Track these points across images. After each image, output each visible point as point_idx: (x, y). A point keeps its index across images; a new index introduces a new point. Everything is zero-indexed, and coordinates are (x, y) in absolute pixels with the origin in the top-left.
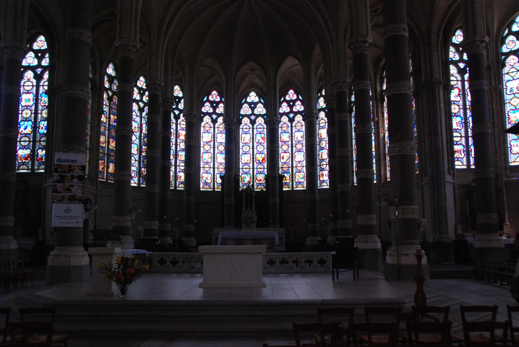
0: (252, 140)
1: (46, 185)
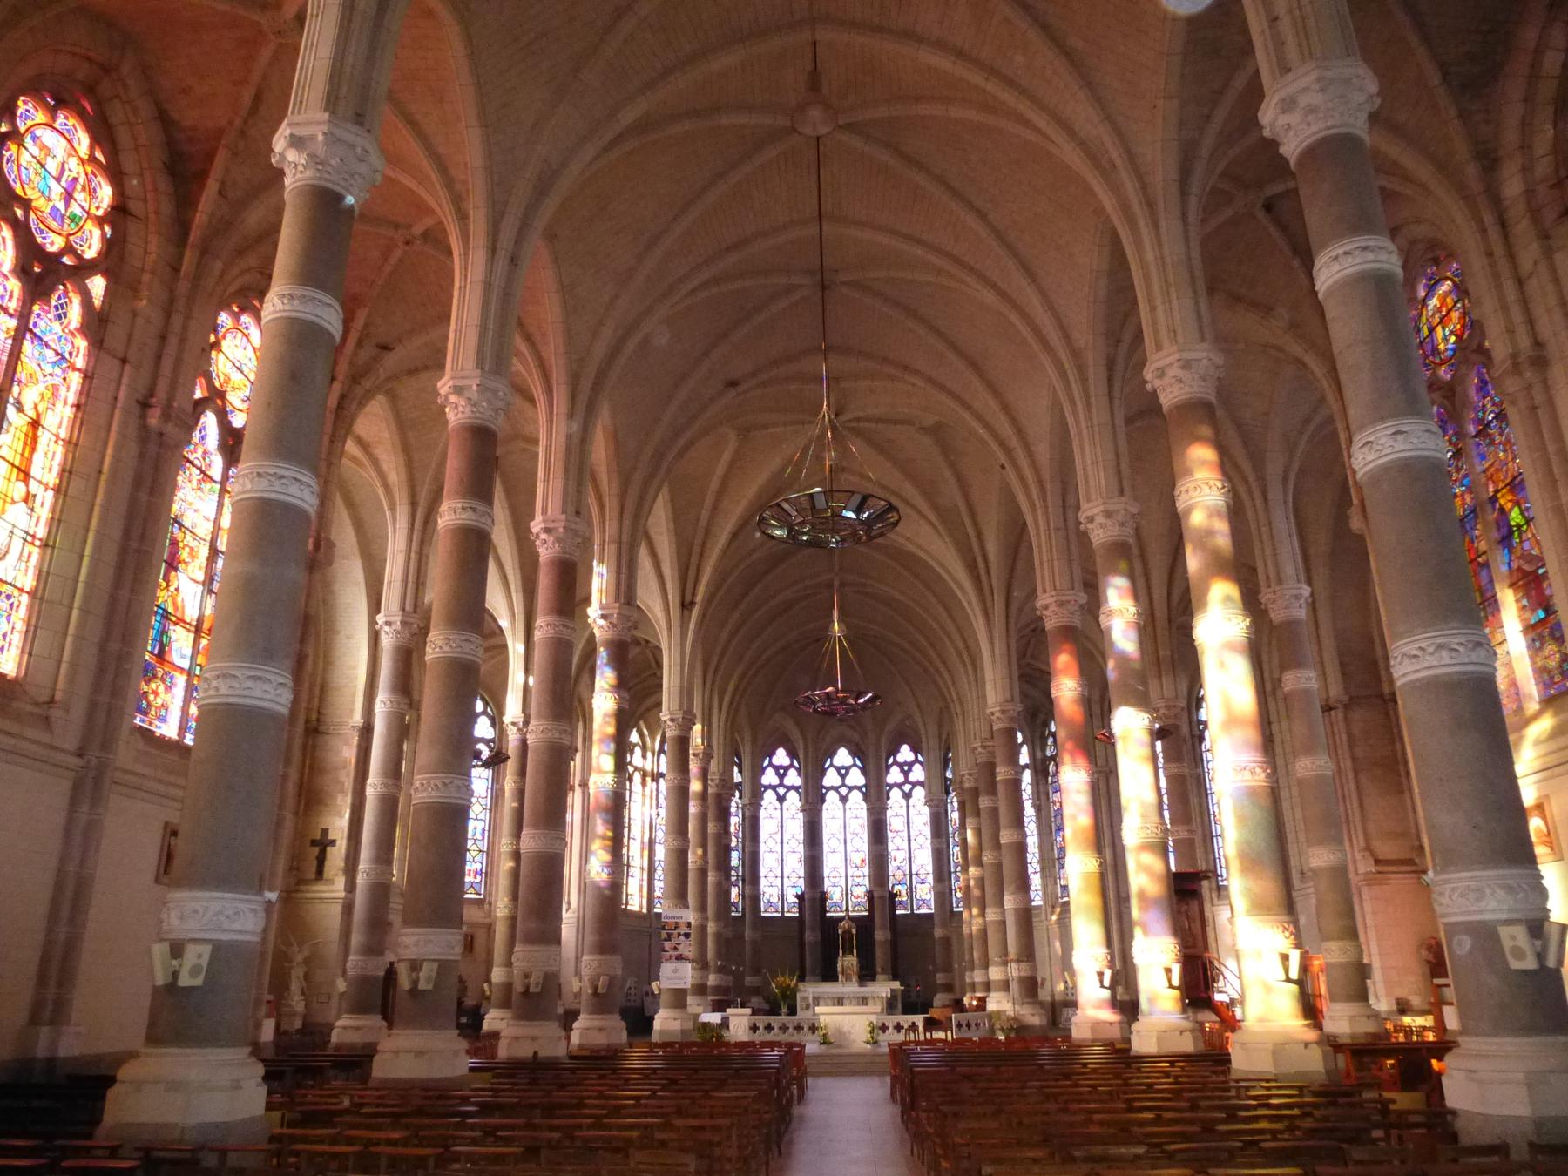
0: (845, 821)
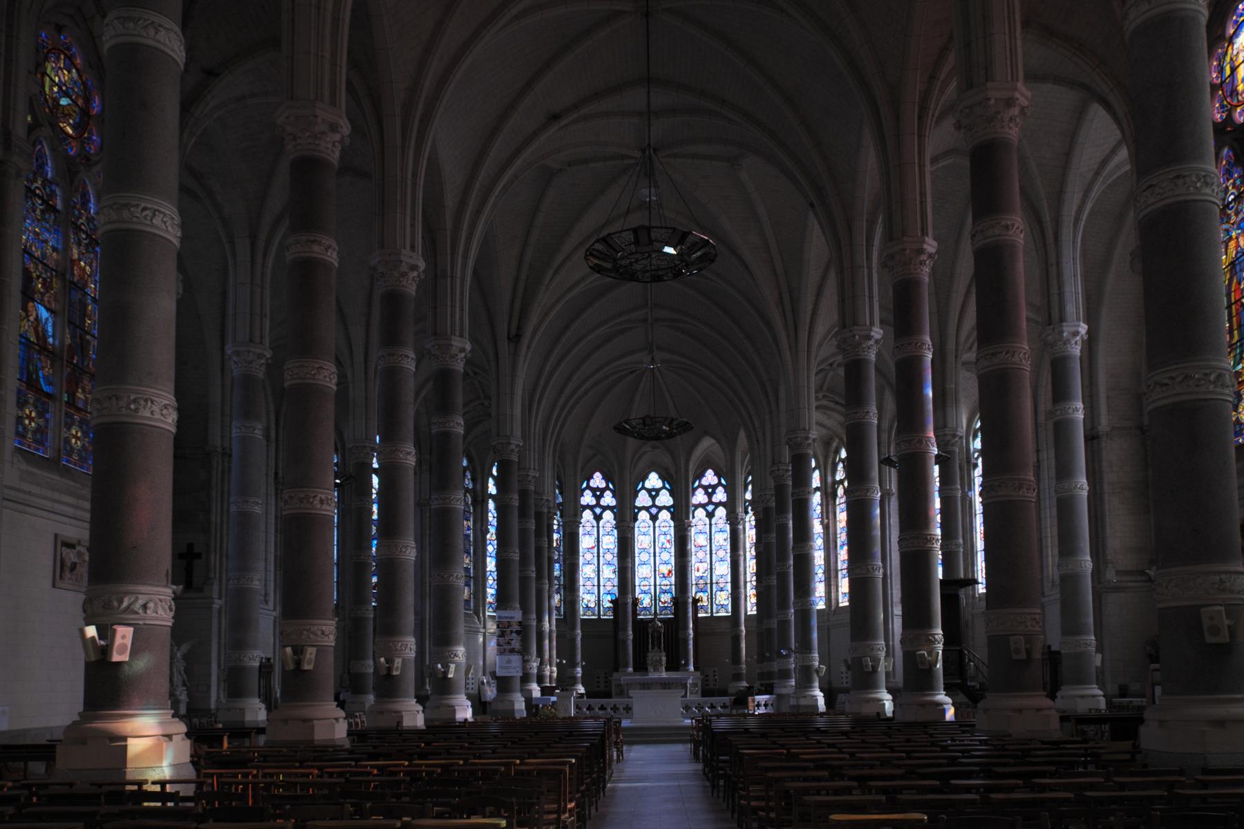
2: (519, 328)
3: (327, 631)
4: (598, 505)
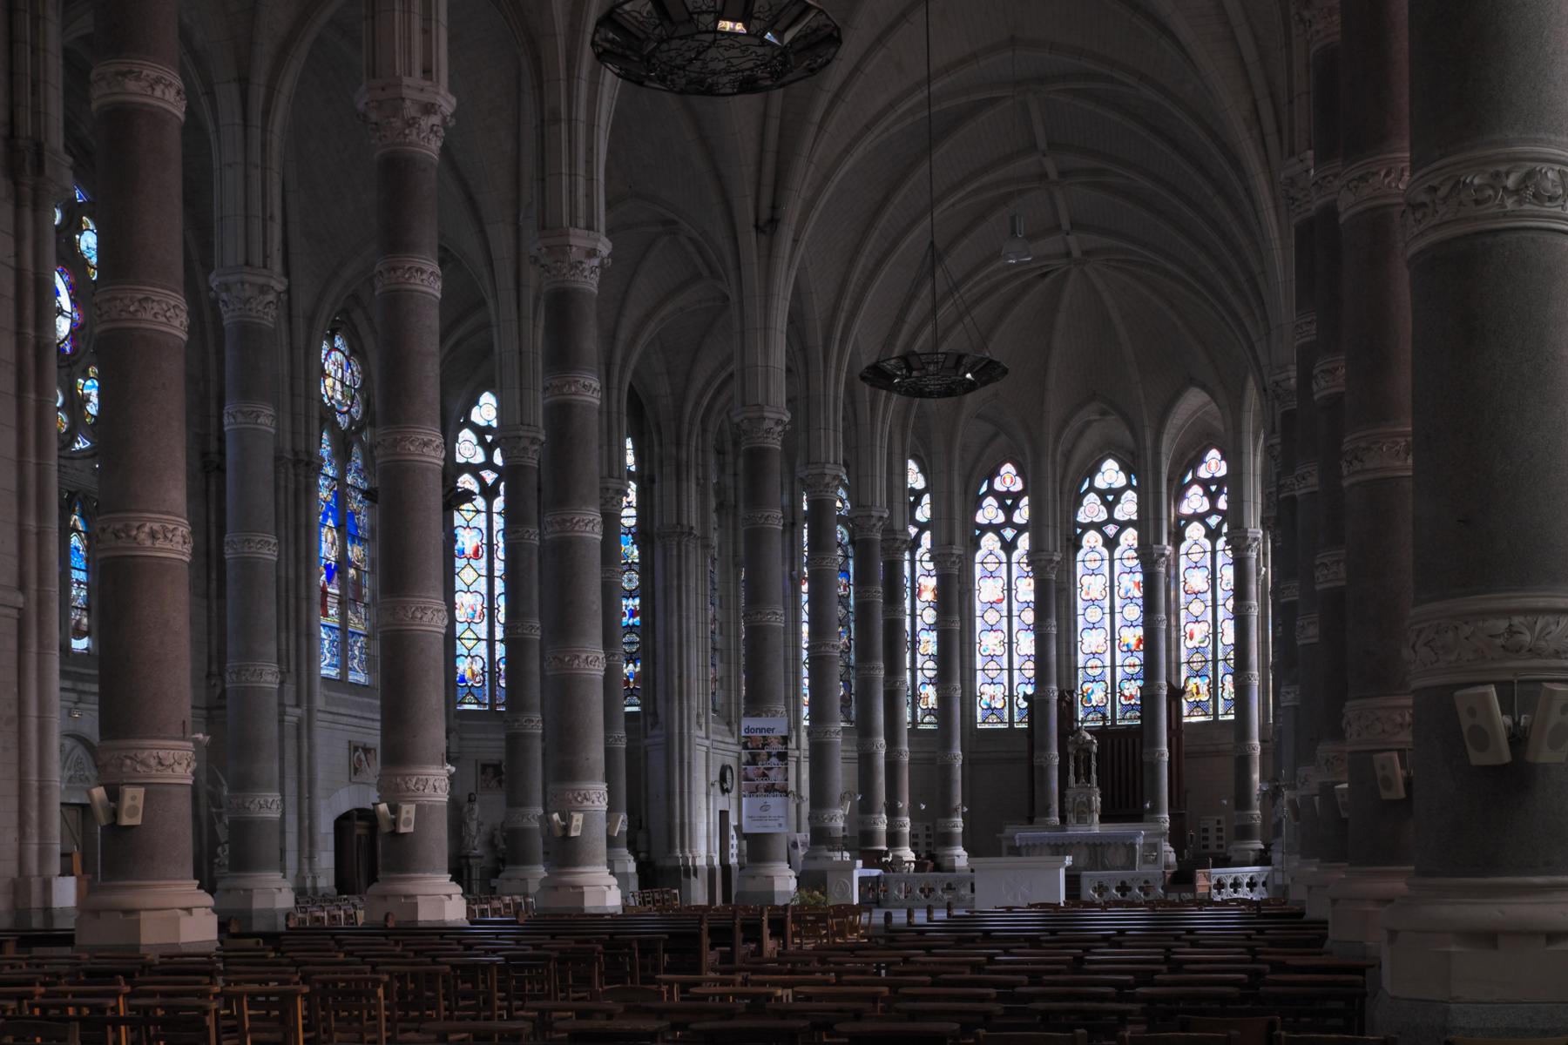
0: (1001, 585)
1: (647, 742)
2: (774, 207)
3: (175, 761)
4: (1009, 522)
